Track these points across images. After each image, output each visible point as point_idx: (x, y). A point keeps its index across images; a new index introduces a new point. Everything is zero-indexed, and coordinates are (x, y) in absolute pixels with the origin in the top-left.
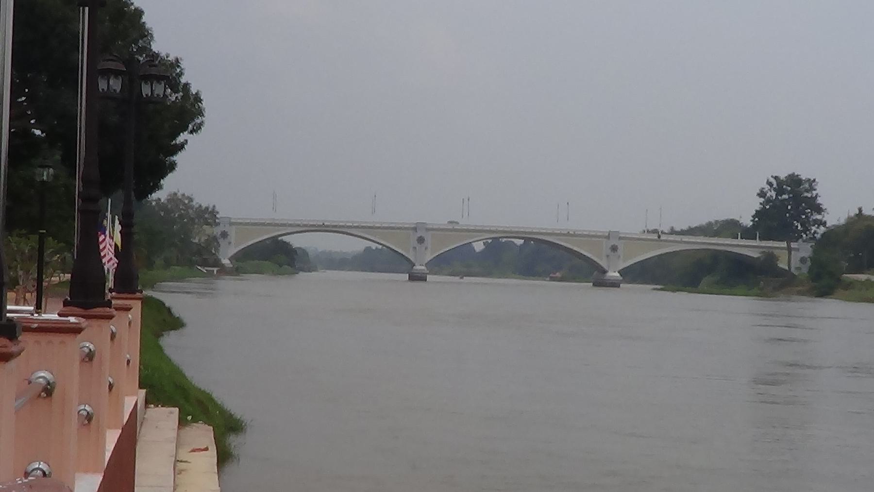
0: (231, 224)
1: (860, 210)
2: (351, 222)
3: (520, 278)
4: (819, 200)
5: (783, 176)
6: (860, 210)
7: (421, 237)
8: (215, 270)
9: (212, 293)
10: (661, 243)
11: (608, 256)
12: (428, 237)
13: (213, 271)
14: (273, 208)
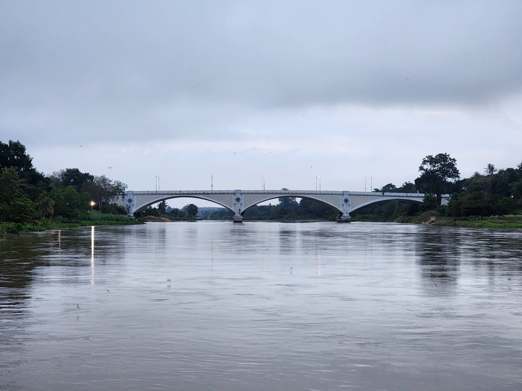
0: (134, 195)
1: (270, 204)
12: (242, 197)
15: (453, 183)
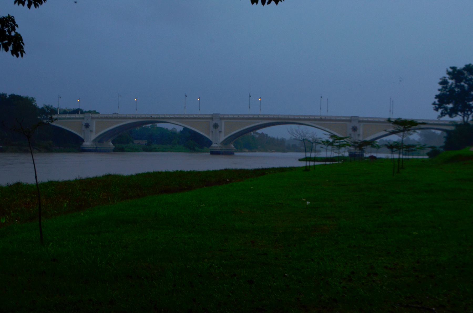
5: (460, 66)
7: (216, 124)
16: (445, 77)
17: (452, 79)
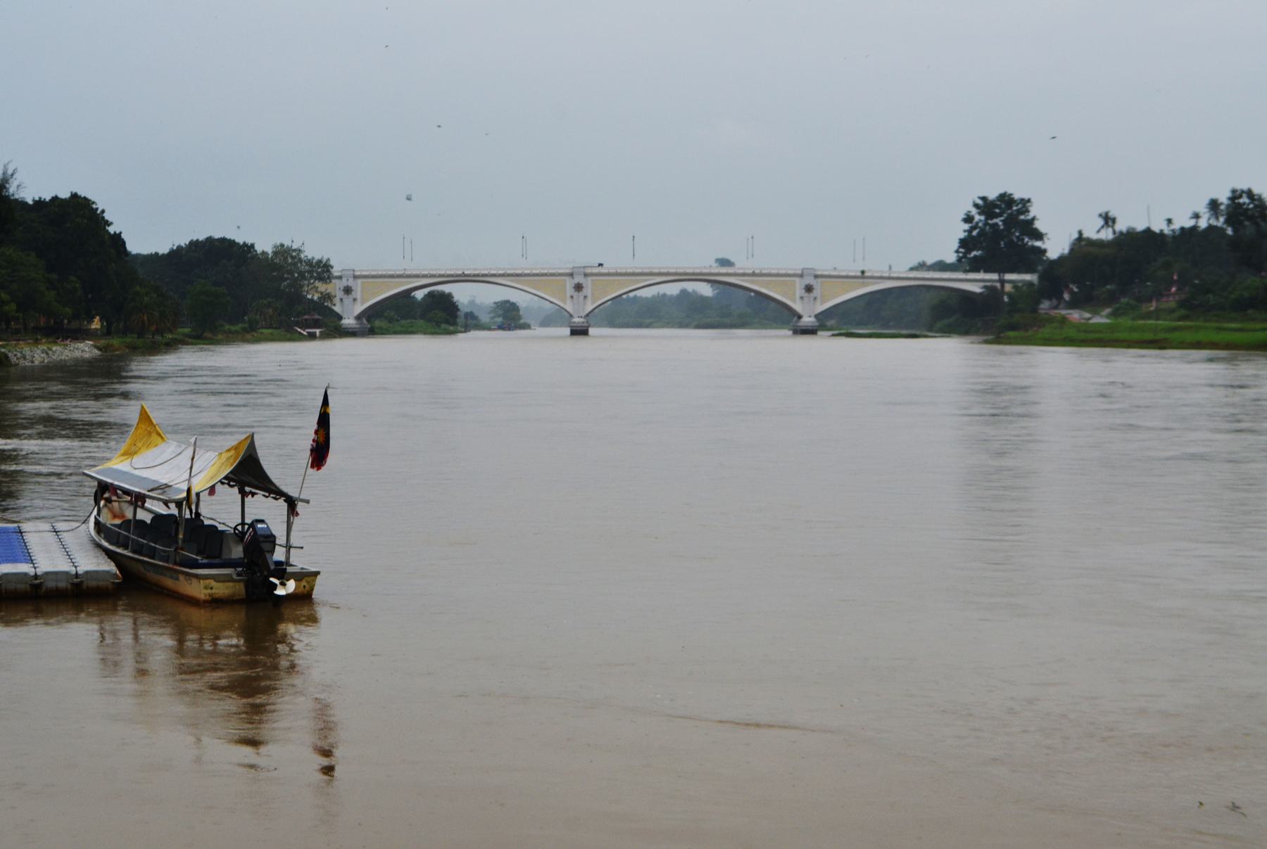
0: (355, 277)
1: (1080, 233)
2: (502, 270)
3: (776, 328)
4: (1038, 225)
5: (992, 195)
6: (1080, 233)
7: (578, 284)
8: (318, 331)
9: (162, 359)
10: (866, 280)
11: (572, 297)
12: (588, 283)
13: (316, 332)
14: (523, 256)
15: (98, 212)
16: (969, 212)
17: (980, 214)
